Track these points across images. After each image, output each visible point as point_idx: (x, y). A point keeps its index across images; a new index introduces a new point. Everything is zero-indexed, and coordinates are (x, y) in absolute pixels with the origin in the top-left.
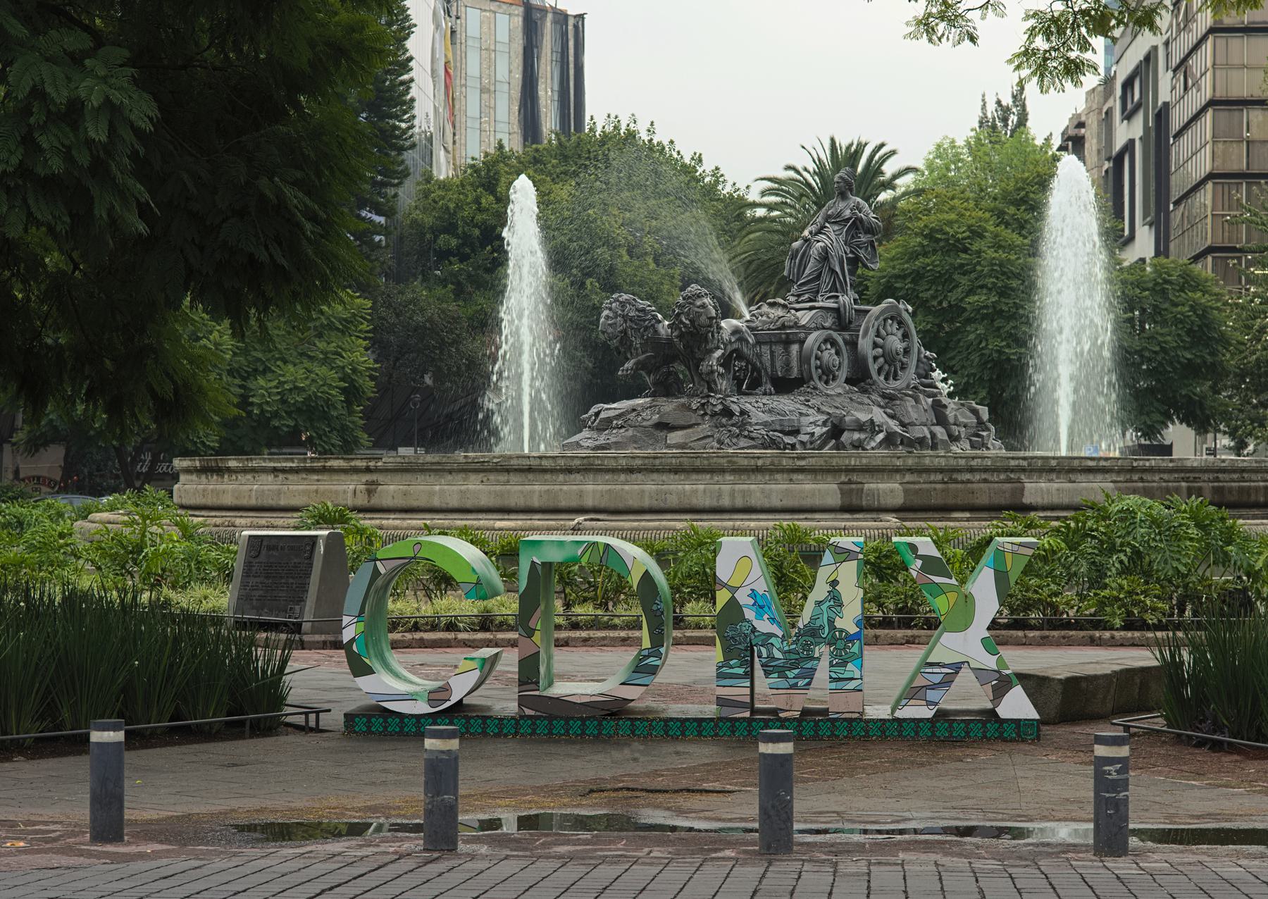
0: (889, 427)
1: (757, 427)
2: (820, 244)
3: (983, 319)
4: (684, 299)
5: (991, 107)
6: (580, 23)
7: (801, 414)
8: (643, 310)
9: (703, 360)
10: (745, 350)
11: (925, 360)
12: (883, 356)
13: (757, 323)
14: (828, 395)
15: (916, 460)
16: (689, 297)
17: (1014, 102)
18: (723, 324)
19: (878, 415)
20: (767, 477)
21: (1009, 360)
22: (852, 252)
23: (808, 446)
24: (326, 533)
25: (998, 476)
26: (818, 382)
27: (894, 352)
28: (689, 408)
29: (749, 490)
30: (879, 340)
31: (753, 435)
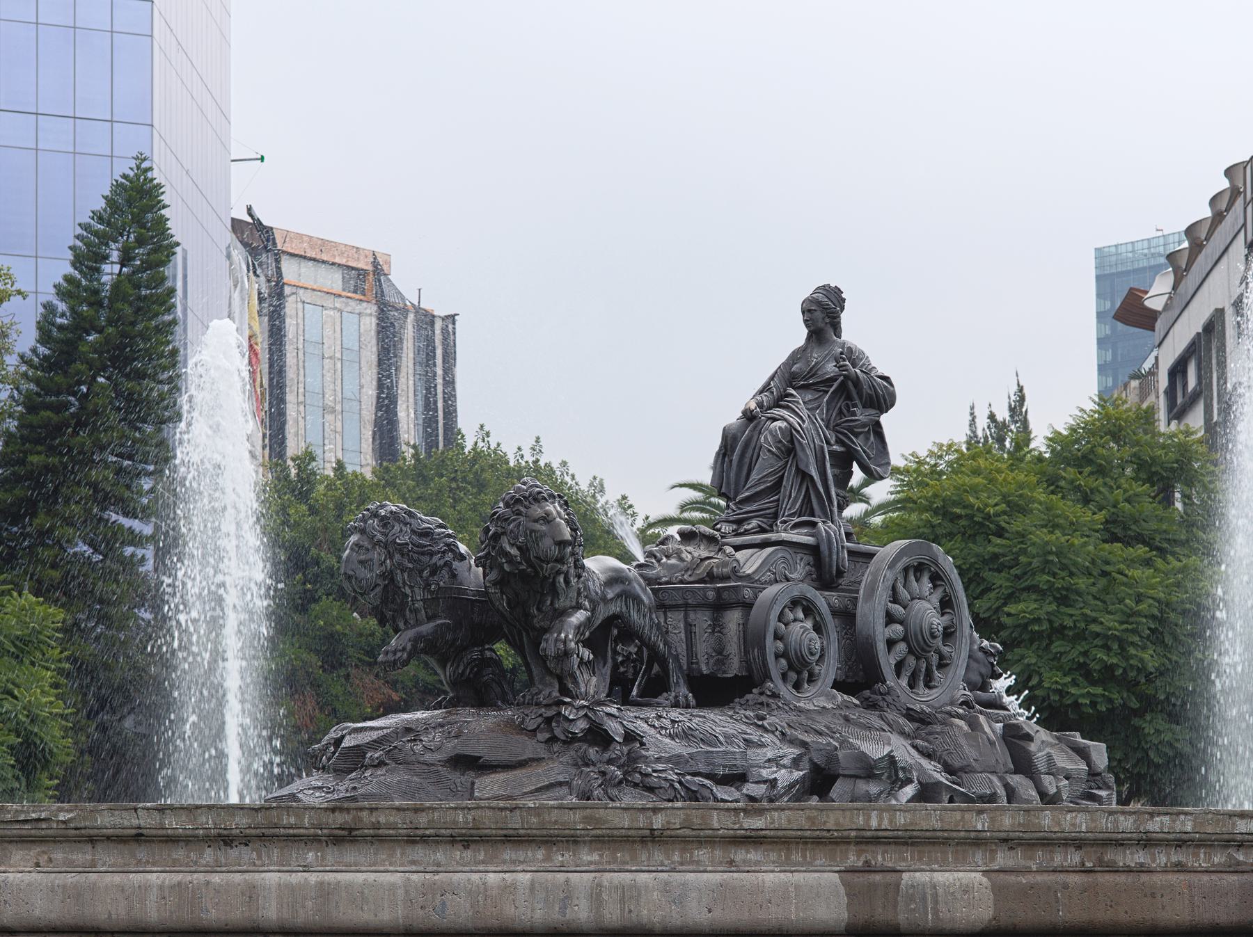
0: (921, 770)
1: (659, 767)
2: (778, 424)
3: (1032, 641)
4: (507, 505)
5: (982, 423)
6: (450, 326)
7: (748, 742)
8: (426, 533)
9: (546, 630)
10: (634, 616)
11: (980, 654)
12: (905, 639)
13: (657, 571)
14: (801, 711)
15: (1021, 818)
16: (518, 501)
17: (1011, 416)
18: (590, 563)
19: (904, 752)
20: (676, 857)
21: (1076, 705)
22: (839, 441)
25: (1208, 858)
26: (779, 682)
28: (521, 729)
29: (634, 886)
30: (897, 609)
31: (653, 781)
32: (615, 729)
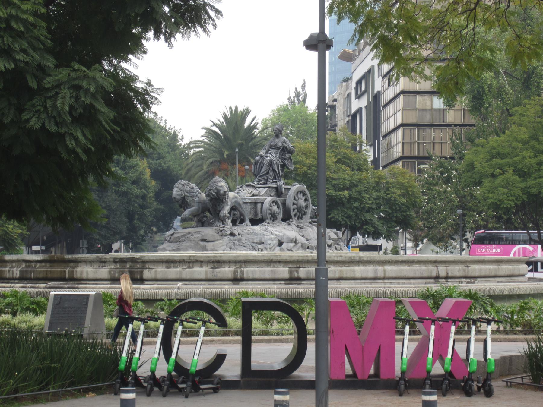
2: (268, 158)
22: (282, 162)
23: (269, 250)
24: (94, 293)
27: (302, 207)
30: (295, 202)
32: (236, 233)
